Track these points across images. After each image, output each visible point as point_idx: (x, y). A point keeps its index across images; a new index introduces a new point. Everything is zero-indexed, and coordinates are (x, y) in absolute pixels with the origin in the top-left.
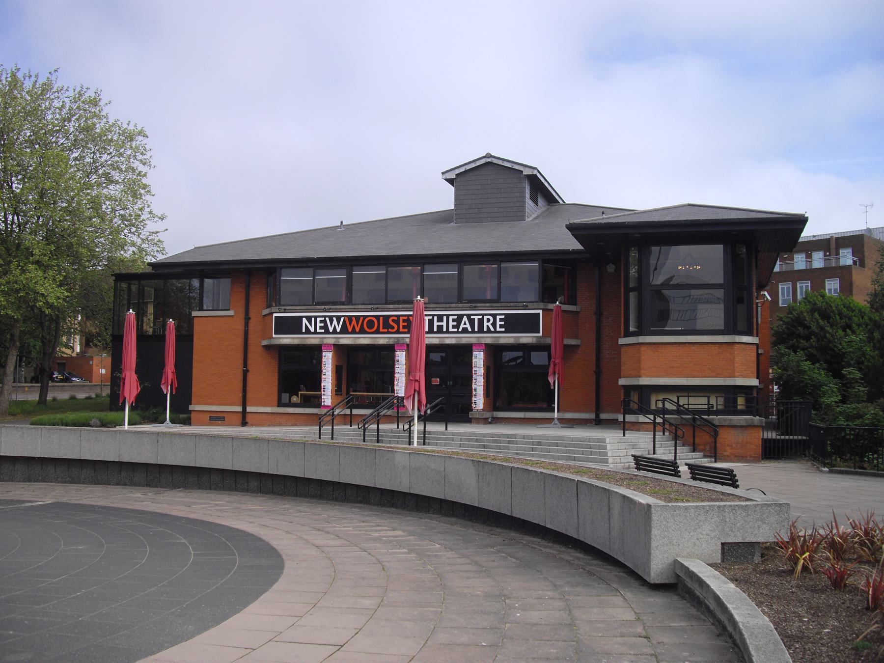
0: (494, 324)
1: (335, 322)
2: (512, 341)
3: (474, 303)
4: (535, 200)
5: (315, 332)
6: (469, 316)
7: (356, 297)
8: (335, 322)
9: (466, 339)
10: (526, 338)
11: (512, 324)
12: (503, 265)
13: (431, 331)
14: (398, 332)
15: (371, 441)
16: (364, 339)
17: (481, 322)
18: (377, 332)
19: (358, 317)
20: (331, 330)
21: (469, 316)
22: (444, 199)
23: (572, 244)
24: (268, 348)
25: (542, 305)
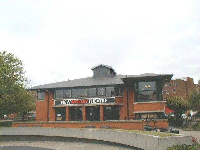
0: (105, 101)
1: (69, 101)
2: (109, 104)
3: (101, 96)
4: (111, 73)
5: (64, 104)
6: (99, 99)
7: (73, 96)
8: (69, 101)
9: (99, 104)
10: (112, 104)
11: (109, 101)
12: (81, 89)
13: (90, 103)
14: (83, 103)
15: (52, 120)
16: (76, 105)
17: (102, 100)
18: (78, 103)
19: (74, 100)
20: (68, 103)
21: (99, 99)
22: (91, 74)
23: (122, 82)
24: (53, 108)
25: (115, 96)
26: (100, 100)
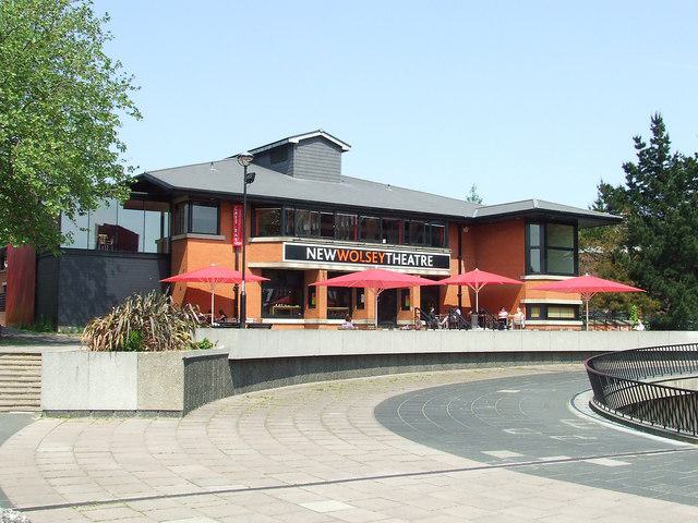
5: (317, 260)
20: (327, 258)
26: (417, 256)
